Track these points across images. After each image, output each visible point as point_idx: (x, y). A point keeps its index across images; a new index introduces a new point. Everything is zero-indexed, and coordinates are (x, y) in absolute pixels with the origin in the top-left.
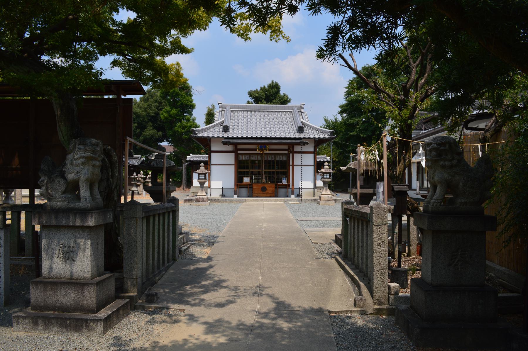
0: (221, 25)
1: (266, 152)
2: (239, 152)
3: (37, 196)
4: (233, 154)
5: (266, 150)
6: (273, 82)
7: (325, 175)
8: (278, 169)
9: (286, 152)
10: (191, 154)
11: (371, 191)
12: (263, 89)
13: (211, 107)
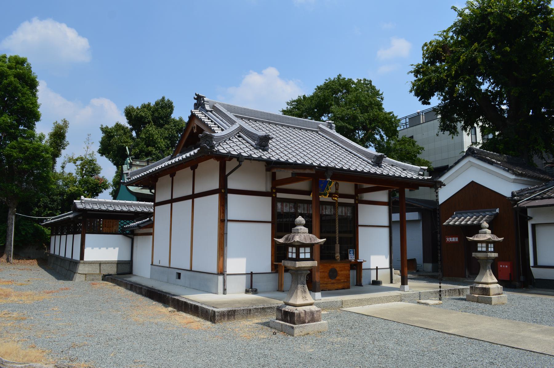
0: (454, 8)
1: (323, 198)
2: (279, 195)
3: (532, 267)
4: (269, 200)
5: (325, 195)
6: (163, 98)
7: (302, 250)
8: (335, 232)
9: (352, 201)
10: (82, 197)
11: (144, 293)
12: (146, 107)
13: (61, 123)
